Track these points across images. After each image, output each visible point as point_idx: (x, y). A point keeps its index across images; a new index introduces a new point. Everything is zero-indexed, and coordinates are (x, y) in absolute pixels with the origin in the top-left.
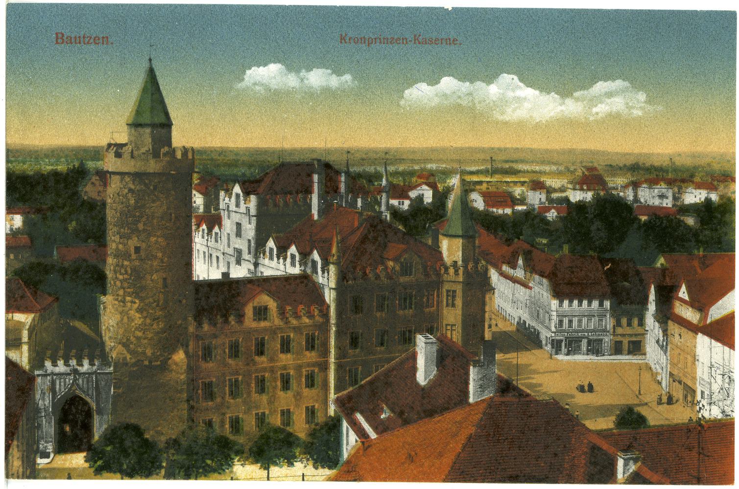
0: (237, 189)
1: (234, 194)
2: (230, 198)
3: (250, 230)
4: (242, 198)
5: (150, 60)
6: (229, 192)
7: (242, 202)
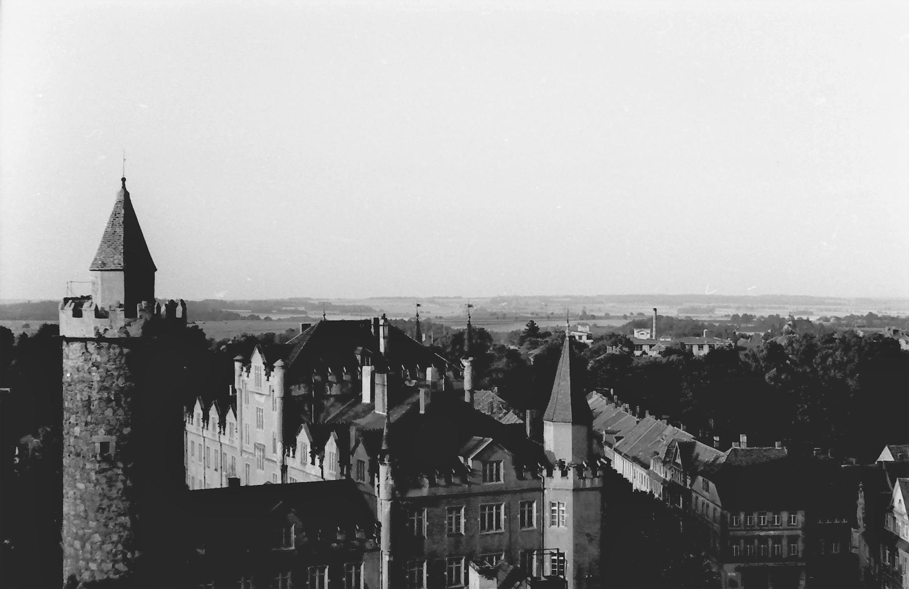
0: (257, 359)
1: (252, 370)
2: (248, 371)
4: (264, 373)
5: (124, 180)
6: (247, 363)
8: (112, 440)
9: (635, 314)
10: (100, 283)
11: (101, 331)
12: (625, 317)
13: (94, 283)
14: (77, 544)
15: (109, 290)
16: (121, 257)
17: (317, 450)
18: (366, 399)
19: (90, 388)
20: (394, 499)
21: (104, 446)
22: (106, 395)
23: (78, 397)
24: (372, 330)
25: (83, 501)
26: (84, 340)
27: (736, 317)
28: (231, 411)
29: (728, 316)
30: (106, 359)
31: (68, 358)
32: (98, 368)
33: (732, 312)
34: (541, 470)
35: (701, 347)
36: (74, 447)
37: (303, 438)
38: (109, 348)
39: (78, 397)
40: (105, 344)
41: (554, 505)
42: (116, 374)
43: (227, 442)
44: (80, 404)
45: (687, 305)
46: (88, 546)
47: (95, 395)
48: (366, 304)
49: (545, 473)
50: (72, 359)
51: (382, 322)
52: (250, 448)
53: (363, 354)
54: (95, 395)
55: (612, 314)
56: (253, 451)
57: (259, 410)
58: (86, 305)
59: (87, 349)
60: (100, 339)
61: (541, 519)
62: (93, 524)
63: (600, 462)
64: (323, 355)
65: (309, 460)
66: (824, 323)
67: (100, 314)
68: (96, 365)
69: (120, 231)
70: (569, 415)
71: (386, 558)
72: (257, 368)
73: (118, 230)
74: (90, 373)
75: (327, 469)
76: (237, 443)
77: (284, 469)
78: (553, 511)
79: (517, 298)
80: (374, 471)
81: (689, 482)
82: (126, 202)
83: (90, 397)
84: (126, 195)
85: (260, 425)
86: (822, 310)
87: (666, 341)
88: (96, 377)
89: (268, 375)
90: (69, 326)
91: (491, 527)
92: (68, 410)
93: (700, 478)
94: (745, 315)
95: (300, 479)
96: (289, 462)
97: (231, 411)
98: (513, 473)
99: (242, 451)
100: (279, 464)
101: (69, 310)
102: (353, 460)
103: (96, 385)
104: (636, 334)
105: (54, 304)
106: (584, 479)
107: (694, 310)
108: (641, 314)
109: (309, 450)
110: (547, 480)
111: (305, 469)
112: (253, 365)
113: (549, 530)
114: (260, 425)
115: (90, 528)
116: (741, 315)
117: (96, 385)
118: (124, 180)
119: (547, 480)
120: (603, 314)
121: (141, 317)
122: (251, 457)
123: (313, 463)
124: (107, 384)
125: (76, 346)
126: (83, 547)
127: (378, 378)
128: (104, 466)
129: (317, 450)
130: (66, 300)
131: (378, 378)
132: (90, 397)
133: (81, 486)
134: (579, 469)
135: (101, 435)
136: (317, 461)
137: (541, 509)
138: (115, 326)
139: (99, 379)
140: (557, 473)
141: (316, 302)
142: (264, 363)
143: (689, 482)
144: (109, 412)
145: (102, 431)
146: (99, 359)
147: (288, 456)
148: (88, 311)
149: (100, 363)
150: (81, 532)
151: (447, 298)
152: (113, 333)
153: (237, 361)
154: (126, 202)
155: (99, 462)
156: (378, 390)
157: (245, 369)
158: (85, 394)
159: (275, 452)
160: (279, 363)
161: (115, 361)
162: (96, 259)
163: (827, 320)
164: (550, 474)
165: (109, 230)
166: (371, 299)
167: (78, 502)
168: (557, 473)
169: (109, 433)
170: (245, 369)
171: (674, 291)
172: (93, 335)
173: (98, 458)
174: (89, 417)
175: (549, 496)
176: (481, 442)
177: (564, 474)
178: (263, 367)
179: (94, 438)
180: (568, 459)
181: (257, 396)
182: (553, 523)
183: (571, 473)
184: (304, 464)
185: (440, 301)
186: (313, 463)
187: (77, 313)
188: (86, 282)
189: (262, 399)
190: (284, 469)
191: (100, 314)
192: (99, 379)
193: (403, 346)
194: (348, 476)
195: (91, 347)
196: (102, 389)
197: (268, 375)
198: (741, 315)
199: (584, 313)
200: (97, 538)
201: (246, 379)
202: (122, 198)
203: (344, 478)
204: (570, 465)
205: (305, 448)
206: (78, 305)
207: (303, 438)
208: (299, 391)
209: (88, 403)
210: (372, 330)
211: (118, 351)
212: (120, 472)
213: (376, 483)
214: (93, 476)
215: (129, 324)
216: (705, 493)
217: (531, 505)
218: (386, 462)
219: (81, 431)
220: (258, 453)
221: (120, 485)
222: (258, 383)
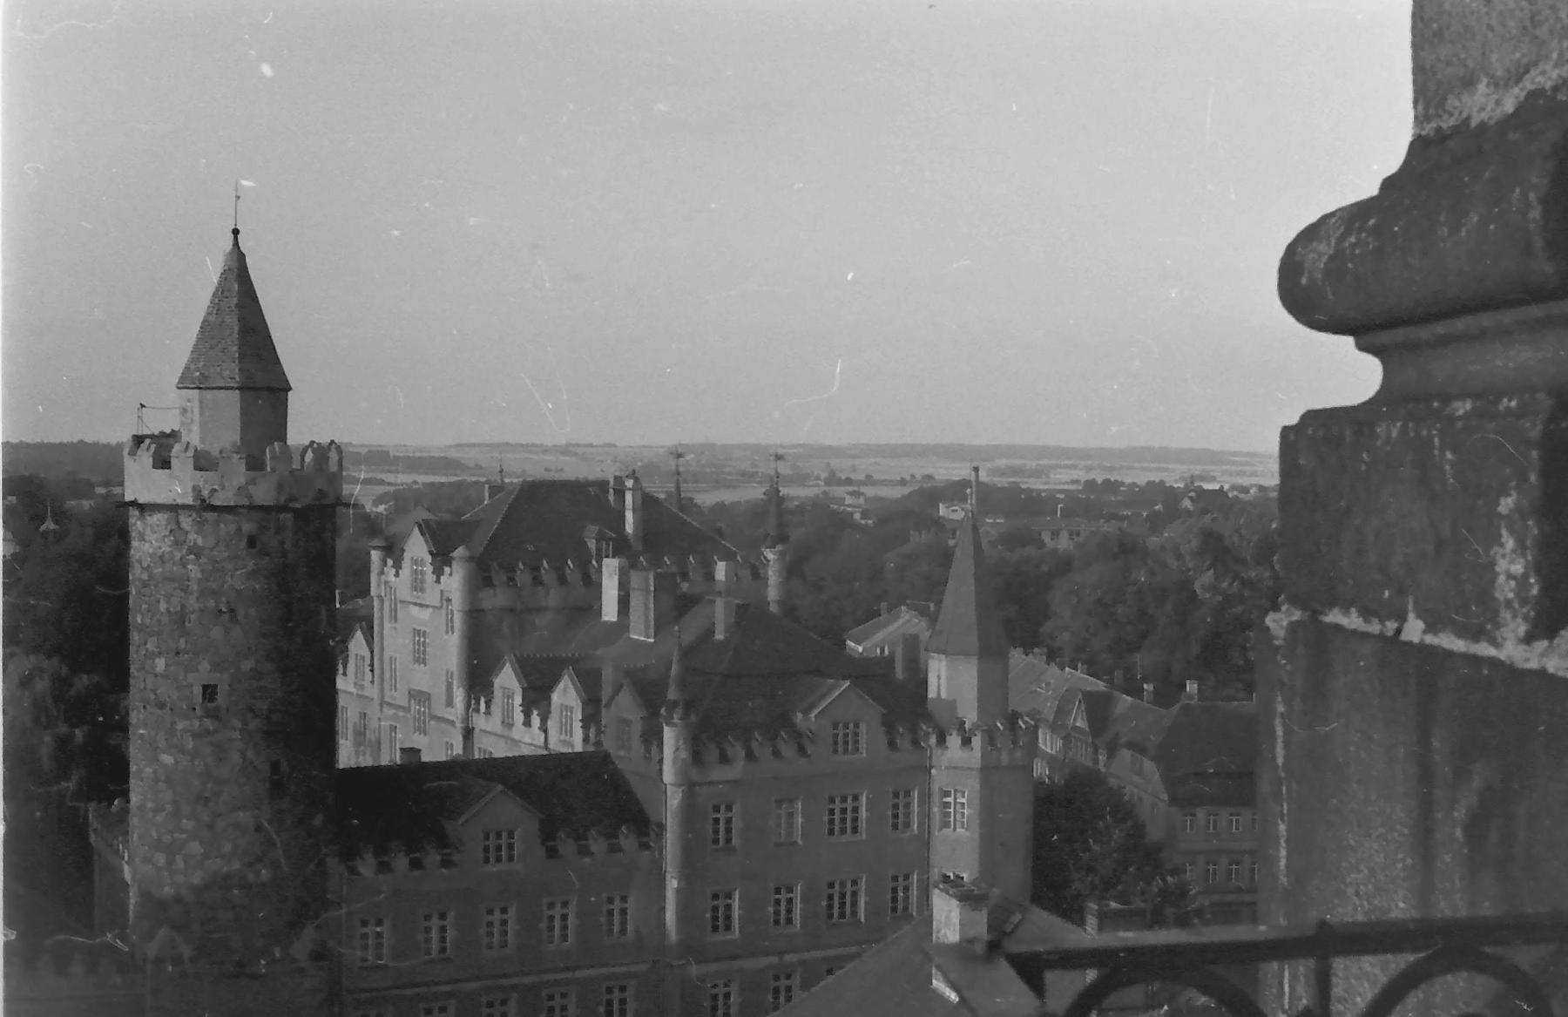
0: (417, 548)
1: (406, 564)
2: (398, 566)
3: (449, 650)
4: (429, 569)
5: (236, 232)
7: (430, 577)
8: (223, 682)
9: (919, 477)
10: (197, 411)
11: (205, 493)
12: (903, 482)
13: (184, 411)
14: (161, 859)
15: (214, 423)
16: (235, 367)
17: (537, 696)
18: (610, 613)
19: (185, 591)
20: (690, 787)
21: (209, 692)
22: (212, 603)
23: (163, 606)
24: (611, 497)
25: (169, 781)
26: (173, 508)
27: (1090, 484)
28: (359, 634)
29: (1076, 482)
30: (212, 541)
31: (142, 538)
32: (198, 556)
33: (1083, 476)
34: (927, 734)
35: (1055, 534)
36: (154, 691)
37: (507, 680)
38: (217, 523)
39: (163, 606)
40: (211, 516)
41: (947, 794)
42: (229, 566)
43: (352, 689)
44: (165, 619)
45: (1002, 463)
46: (179, 862)
47: (193, 603)
48: (454, 454)
49: (933, 740)
50: (149, 542)
51: (630, 483)
52: (401, 698)
53: (600, 539)
54: (193, 603)
55: (877, 476)
56: (404, 703)
57: (417, 632)
58: (177, 448)
59: (178, 523)
60: (204, 506)
61: (926, 815)
62: (187, 824)
63: (1025, 722)
64: (529, 538)
65: (519, 717)
66: (1242, 496)
67: (202, 462)
68: (196, 551)
69: (232, 321)
70: (973, 641)
71: (672, 884)
72: (415, 562)
73: (228, 320)
74: (184, 566)
75: (562, 729)
76: (372, 692)
77: (468, 733)
78: (947, 805)
79: (711, 447)
80: (652, 737)
81: (1102, 758)
82: (238, 274)
83: (183, 607)
84: (241, 257)
85: (420, 658)
86: (1231, 474)
87: (994, 524)
88: (194, 571)
89: (438, 572)
90: (142, 482)
91: (843, 831)
92: (142, 629)
93: (1126, 754)
94: (1107, 481)
95: (500, 751)
96: (479, 722)
97: (359, 634)
98: (882, 741)
99: (383, 703)
100: (459, 725)
101: (146, 456)
102: (606, 716)
103: (194, 586)
104: (943, 510)
105: (115, 451)
106: (999, 750)
107: (1015, 471)
108: (930, 477)
109: (518, 700)
110: (937, 752)
111: (512, 731)
112: (407, 556)
113: (941, 836)
114: (420, 658)
115: (183, 831)
116: (1099, 481)
117: (194, 586)
118: (236, 232)
119: (937, 752)
120: (862, 477)
121: (273, 470)
122: (401, 714)
123: (527, 723)
124: (214, 585)
125: (158, 518)
126: (170, 862)
127: (635, 579)
128: (209, 724)
129: (537, 696)
130: (139, 440)
131: (635, 579)
132: (183, 607)
133: (167, 759)
134: (991, 738)
135: (204, 672)
136: (536, 720)
137: (926, 798)
138: (229, 486)
139: (199, 575)
140: (954, 740)
141: (364, 451)
142: (431, 553)
143: (1102, 758)
144: (217, 633)
145: (205, 666)
146: (200, 542)
147: (478, 711)
148: (181, 461)
149: (202, 548)
150: (166, 838)
151: (591, 446)
152: (224, 498)
153: (375, 548)
154: (238, 274)
155: (200, 719)
156: (636, 601)
157: (390, 562)
158: (176, 601)
159: (450, 702)
160: (460, 552)
161: (227, 546)
162: (187, 368)
163: (1245, 490)
164: (942, 740)
165: (212, 319)
166: (459, 446)
167: (162, 786)
168: (954, 740)
169: (216, 667)
170: (390, 562)
171: (1076, 440)
172: (189, 500)
173: (199, 711)
174: (182, 641)
175: (939, 778)
176: (832, 688)
177: (966, 742)
178: (429, 558)
179: (191, 677)
180: (970, 716)
181: (414, 610)
182: (946, 825)
183: (977, 741)
184: (508, 723)
185: (579, 450)
186: (527, 723)
187: (163, 463)
188: (169, 409)
189: (425, 615)
190: (468, 733)
191: (202, 462)
192: (199, 575)
193: (669, 527)
194: (598, 743)
195: (187, 522)
196: (203, 594)
197: (438, 572)
198: (1099, 481)
199: (833, 474)
200: (196, 848)
201: (392, 578)
202: (235, 264)
203: (592, 749)
204: (976, 727)
205: (509, 696)
206: (161, 448)
207: (507, 680)
208: (495, 599)
209: (180, 618)
210: (611, 497)
211: (232, 527)
212: (236, 735)
213: (656, 757)
214: (190, 744)
215: (253, 482)
216: (1136, 779)
217: (908, 794)
218: (676, 720)
219: (167, 665)
220: (415, 707)
221: (236, 757)
222: (418, 585)
